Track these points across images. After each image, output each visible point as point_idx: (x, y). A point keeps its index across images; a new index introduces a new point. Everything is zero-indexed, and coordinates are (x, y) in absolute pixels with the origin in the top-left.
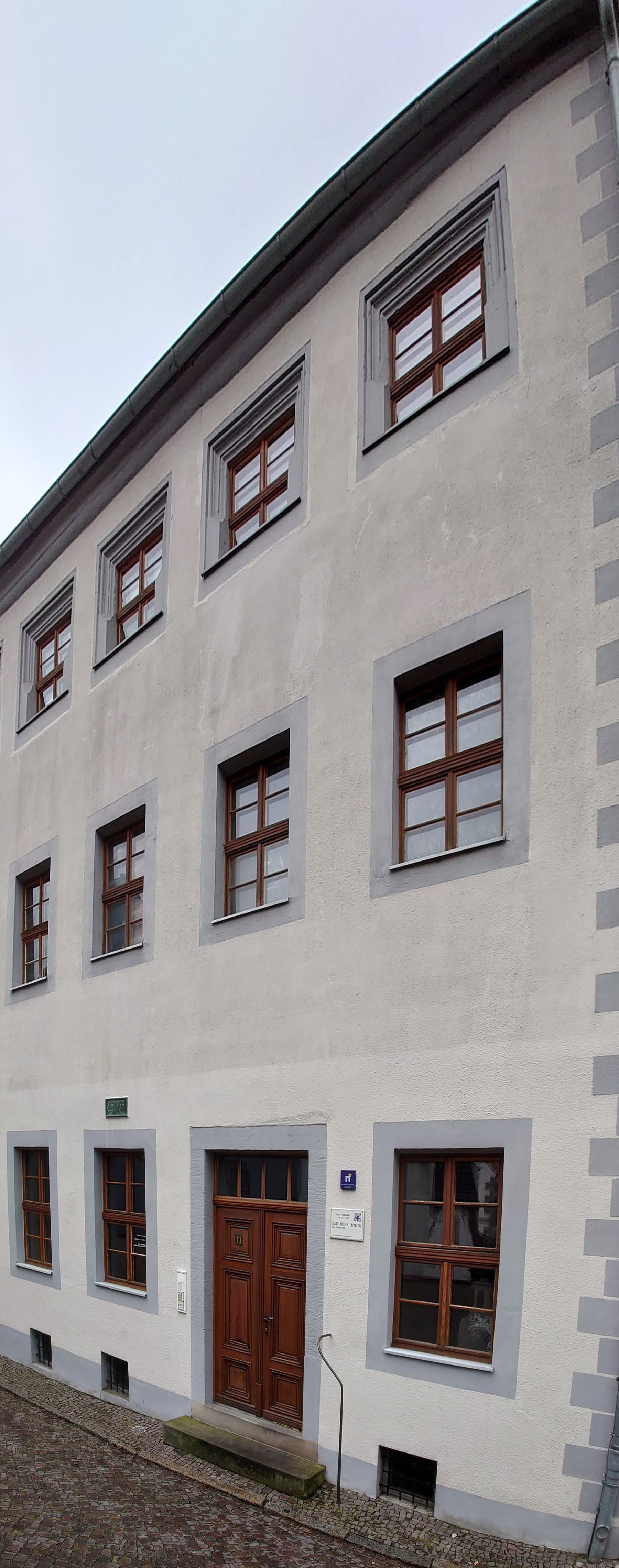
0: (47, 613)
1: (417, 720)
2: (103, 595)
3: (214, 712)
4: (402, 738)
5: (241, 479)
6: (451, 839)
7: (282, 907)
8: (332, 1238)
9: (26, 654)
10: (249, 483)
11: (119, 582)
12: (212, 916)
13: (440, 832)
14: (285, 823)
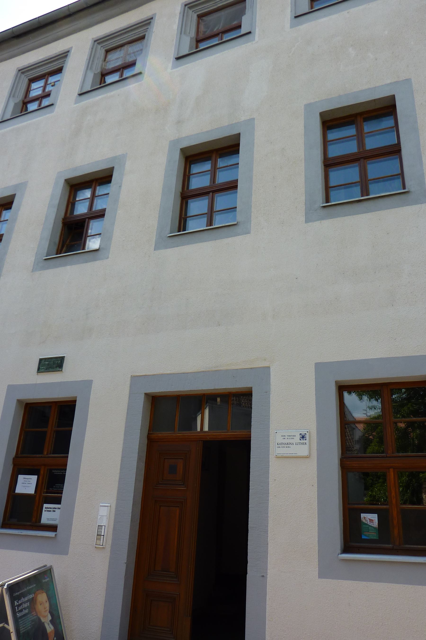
0: (35, 68)
1: (196, 169)
2: (93, 61)
3: (179, 122)
4: (325, 143)
5: (34, 86)
6: (210, 222)
7: (232, 228)
8: (277, 457)
9: (17, 86)
10: (37, 89)
11: (29, 86)
12: (45, 255)
13: (204, 220)
14: (104, 210)
